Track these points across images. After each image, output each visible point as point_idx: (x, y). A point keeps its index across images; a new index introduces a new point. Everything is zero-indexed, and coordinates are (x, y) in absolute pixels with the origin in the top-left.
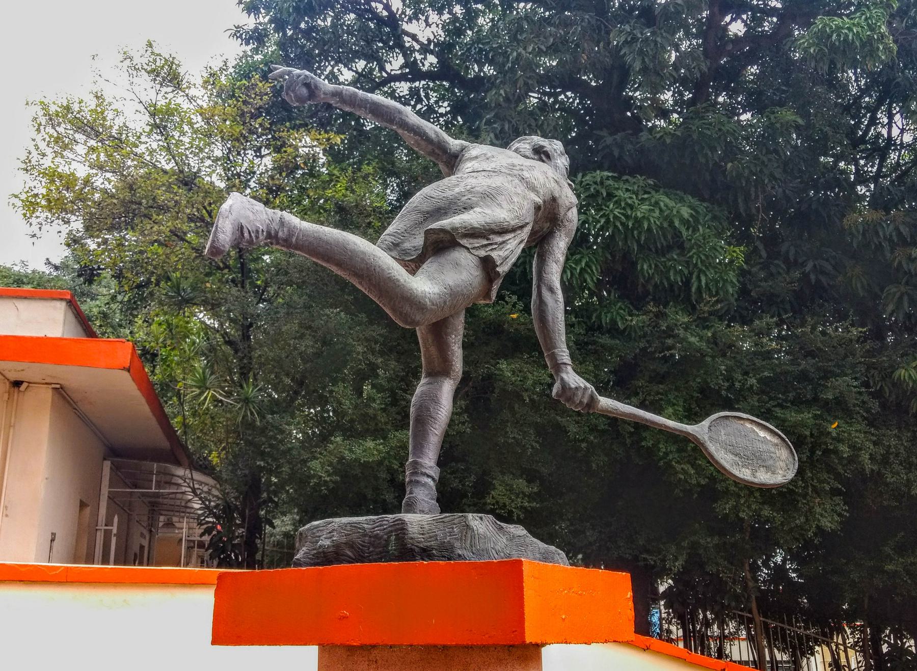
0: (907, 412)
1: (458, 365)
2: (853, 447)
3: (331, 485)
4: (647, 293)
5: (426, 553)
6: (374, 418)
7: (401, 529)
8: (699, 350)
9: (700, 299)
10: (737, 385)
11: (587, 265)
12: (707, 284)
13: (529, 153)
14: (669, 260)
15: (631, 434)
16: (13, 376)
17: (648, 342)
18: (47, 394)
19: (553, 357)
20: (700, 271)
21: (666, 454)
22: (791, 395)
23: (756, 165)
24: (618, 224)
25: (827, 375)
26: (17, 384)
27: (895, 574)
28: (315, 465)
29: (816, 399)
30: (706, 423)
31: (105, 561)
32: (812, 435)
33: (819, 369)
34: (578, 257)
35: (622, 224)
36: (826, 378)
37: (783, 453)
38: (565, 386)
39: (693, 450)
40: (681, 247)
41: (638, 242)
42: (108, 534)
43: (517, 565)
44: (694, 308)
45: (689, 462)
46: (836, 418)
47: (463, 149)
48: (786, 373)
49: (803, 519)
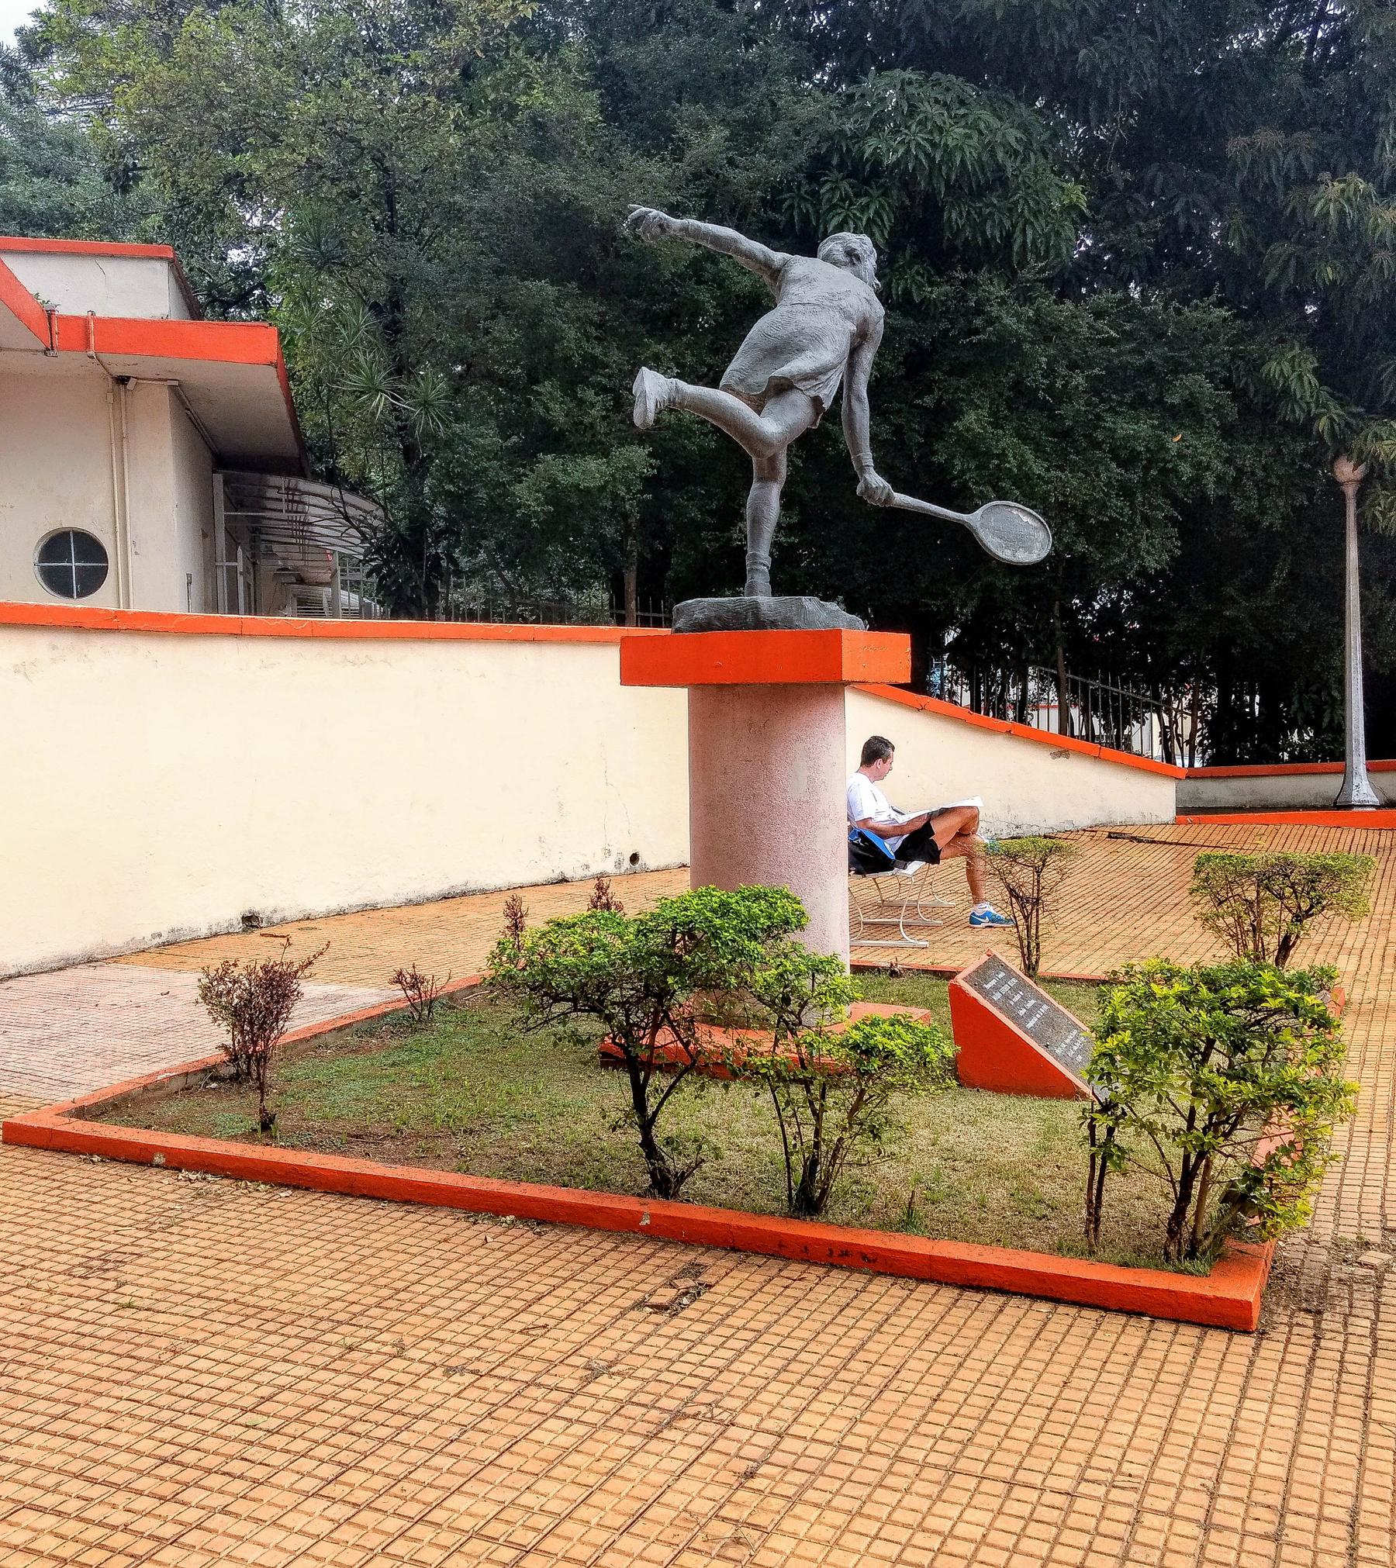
0: (1274, 416)
1: (783, 470)
2: (1198, 466)
3: (542, 517)
4: (955, 250)
5: (774, 624)
6: (592, 426)
7: (755, 606)
8: (1016, 335)
9: (1023, 263)
10: (1059, 384)
11: (876, 212)
12: (1034, 242)
13: (840, 256)
14: (987, 206)
15: (920, 445)
16: (119, 371)
17: (950, 321)
18: (163, 395)
19: (859, 460)
20: (1027, 221)
21: (963, 472)
22: (1128, 397)
23: (1120, 54)
24: (922, 157)
25: (1178, 368)
26: (122, 380)
27: (1234, 621)
28: (520, 489)
29: (1160, 401)
30: (979, 512)
31: (233, 608)
32: (1148, 450)
33: (1166, 360)
34: (864, 200)
35: (927, 155)
36: (1175, 372)
37: (1041, 535)
38: (867, 487)
39: (965, 536)
40: (1003, 182)
41: (947, 182)
42: (232, 572)
43: (838, 633)
44: (1014, 273)
45: (990, 483)
46: (1182, 426)
47: (786, 263)
48: (1124, 367)
49: (1124, 556)
